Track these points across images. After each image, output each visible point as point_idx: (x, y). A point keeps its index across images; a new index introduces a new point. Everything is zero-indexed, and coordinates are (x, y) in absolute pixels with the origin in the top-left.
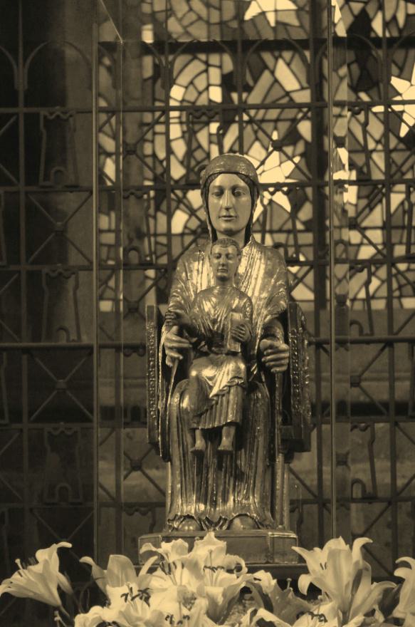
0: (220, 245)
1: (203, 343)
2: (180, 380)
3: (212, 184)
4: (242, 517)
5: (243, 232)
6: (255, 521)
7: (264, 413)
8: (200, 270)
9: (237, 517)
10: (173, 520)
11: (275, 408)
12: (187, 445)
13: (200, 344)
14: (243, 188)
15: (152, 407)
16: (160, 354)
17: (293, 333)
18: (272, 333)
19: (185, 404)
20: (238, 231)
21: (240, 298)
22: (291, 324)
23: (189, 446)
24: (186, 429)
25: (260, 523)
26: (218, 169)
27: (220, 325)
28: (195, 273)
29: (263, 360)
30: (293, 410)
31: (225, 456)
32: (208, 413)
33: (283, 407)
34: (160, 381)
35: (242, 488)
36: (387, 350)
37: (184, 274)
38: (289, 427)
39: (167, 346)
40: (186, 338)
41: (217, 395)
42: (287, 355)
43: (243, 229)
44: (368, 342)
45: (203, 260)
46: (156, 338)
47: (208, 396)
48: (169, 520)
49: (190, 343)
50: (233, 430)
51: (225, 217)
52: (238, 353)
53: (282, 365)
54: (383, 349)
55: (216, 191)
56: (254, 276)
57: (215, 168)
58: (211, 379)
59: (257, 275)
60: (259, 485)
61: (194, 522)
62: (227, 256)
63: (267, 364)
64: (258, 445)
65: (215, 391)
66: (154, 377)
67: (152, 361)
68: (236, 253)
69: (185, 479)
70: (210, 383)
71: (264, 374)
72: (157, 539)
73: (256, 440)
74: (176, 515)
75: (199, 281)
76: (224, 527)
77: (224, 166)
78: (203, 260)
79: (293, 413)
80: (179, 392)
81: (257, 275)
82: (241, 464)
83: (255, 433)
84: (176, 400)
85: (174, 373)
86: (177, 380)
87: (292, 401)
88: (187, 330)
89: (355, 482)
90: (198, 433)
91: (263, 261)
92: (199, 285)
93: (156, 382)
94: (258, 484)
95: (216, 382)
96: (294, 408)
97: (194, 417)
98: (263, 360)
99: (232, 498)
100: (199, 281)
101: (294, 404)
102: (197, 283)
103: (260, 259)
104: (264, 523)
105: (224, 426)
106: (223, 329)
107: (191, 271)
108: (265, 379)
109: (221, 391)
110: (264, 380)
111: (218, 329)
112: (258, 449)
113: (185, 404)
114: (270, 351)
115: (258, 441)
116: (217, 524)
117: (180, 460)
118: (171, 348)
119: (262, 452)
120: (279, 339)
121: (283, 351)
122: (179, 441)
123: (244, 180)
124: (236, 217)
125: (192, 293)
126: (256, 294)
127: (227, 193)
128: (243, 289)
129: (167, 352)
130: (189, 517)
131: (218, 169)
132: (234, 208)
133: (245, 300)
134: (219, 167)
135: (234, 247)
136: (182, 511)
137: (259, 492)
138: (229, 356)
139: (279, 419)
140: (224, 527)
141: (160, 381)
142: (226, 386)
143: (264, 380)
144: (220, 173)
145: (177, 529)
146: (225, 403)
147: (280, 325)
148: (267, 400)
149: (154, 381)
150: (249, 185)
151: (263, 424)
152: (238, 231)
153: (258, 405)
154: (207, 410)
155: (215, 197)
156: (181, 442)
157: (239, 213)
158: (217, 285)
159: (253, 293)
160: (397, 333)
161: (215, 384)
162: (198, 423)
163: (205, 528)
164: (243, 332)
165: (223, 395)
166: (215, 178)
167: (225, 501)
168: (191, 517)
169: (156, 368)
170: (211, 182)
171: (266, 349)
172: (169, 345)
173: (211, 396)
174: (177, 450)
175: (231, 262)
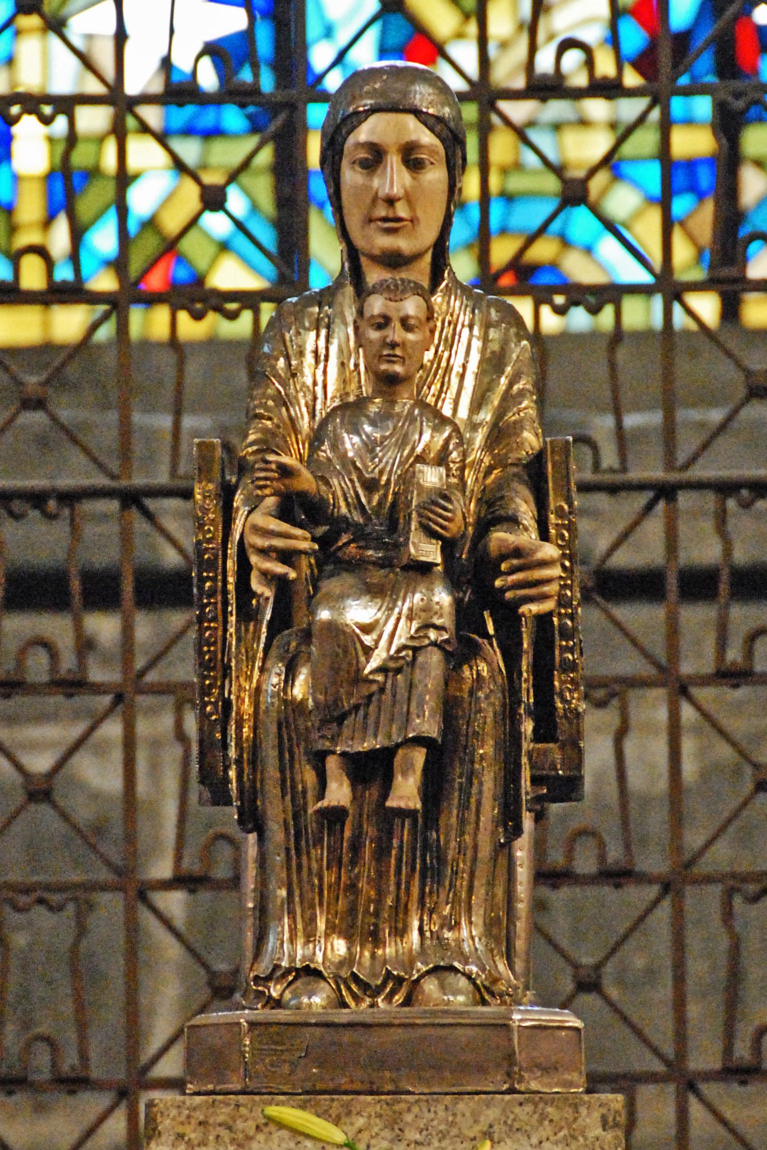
0: (386, 295)
1: (345, 539)
2: (280, 631)
3: (351, 140)
4: (439, 974)
5: (428, 258)
6: (475, 984)
7: (495, 713)
8: (322, 352)
9: (428, 973)
10: (268, 978)
11: (520, 702)
12: (304, 792)
13: (337, 540)
14: (432, 151)
15: (209, 694)
16: (231, 564)
17: (560, 513)
18: (510, 512)
19: (299, 690)
20: (417, 257)
21: (436, 429)
22: (555, 493)
23: (310, 795)
24: (299, 752)
25: (487, 989)
26: (369, 102)
27: (385, 496)
28: (309, 359)
29: (498, 583)
30: (559, 705)
31: (397, 821)
32: (361, 712)
33: (535, 696)
34: (232, 630)
35: (443, 897)
36: (661, 505)
37: (281, 363)
38: (551, 745)
39: (253, 546)
40: (300, 526)
41: (382, 669)
42: (557, 571)
43: (429, 248)
44: (613, 489)
45: (328, 327)
46: (220, 520)
47: (359, 670)
48: (257, 979)
49: (314, 539)
50: (419, 756)
51: (385, 219)
52: (433, 565)
53: (544, 597)
54: (649, 508)
55: (362, 154)
56: (457, 369)
57: (362, 97)
58: (367, 629)
59: (464, 367)
60: (483, 891)
61: (323, 984)
62: (405, 323)
63: (509, 595)
64: (480, 792)
65: (375, 662)
66: (214, 619)
67: (208, 578)
68: (423, 315)
69: (300, 881)
70: (368, 640)
71: (491, 615)
72: (236, 1029)
73: (475, 781)
74: (277, 967)
75: (320, 379)
76: (398, 998)
77: (382, 93)
78: (328, 327)
79: (561, 712)
80: (281, 660)
81: (464, 367)
82: (438, 840)
83: (472, 762)
84: (275, 679)
85: (268, 617)
86: (275, 628)
87: (556, 683)
88: (302, 505)
89: (574, 840)
90: (332, 764)
91: (476, 331)
92: (319, 390)
93: (220, 633)
94: (480, 891)
95: (380, 636)
96: (564, 700)
97: (324, 722)
98: (498, 583)
99: (416, 924)
100: (320, 379)
101: (562, 691)
102: (315, 384)
103: (471, 327)
104: (495, 989)
105: (398, 746)
106: (394, 505)
107: (301, 354)
108: (496, 630)
109: (391, 658)
110: (491, 631)
111: (380, 504)
112: (479, 803)
113: (299, 690)
114: (515, 562)
115: (481, 784)
116: (376, 992)
117: (287, 829)
118: (264, 552)
119: (489, 811)
120: (526, 529)
121: (544, 564)
122: (283, 781)
123: (432, 130)
124: (412, 221)
125: (304, 409)
126: (463, 412)
127: (394, 160)
128: (430, 400)
129: (254, 559)
130: (310, 973)
131: (369, 102)
132: (409, 198)
133: (446, 434)
134: (370, 95)
135: (420, 299)
136: (292, 959)
137: (482, 912)
138: (411, 574)
139: (528, 727)
140: (398, 998)
141: (232, 630)
142: (404, 647)
143: (491, 631)
144: (374, 110)
145: (278, 1004)
146: (402, 692)
147: (525, 492)
148: (499, 680)
149: (216, 629)
150: (443, 141)
151: (491, 742)
152: (417, 257)
153: (481, 694)
154: (356, 708)
155: (359, 169)
156: (287, 784)
157: (420, 213)
158: (377, 393)
159: (455, 410)
160: (686, 467)
161: (377, 642)
162: (334, 739)
163: (349, 1000)
164: (449, 515)
165: (398, 671)
166: (360, 123)
167: (401, 932)
168: (316, 974)
169: (219, 598)
170: (349, 133)
171: (503, 557)
172: (261, 542)
173: (366, 671)
174: (277, 802)
175: (411, 337)
